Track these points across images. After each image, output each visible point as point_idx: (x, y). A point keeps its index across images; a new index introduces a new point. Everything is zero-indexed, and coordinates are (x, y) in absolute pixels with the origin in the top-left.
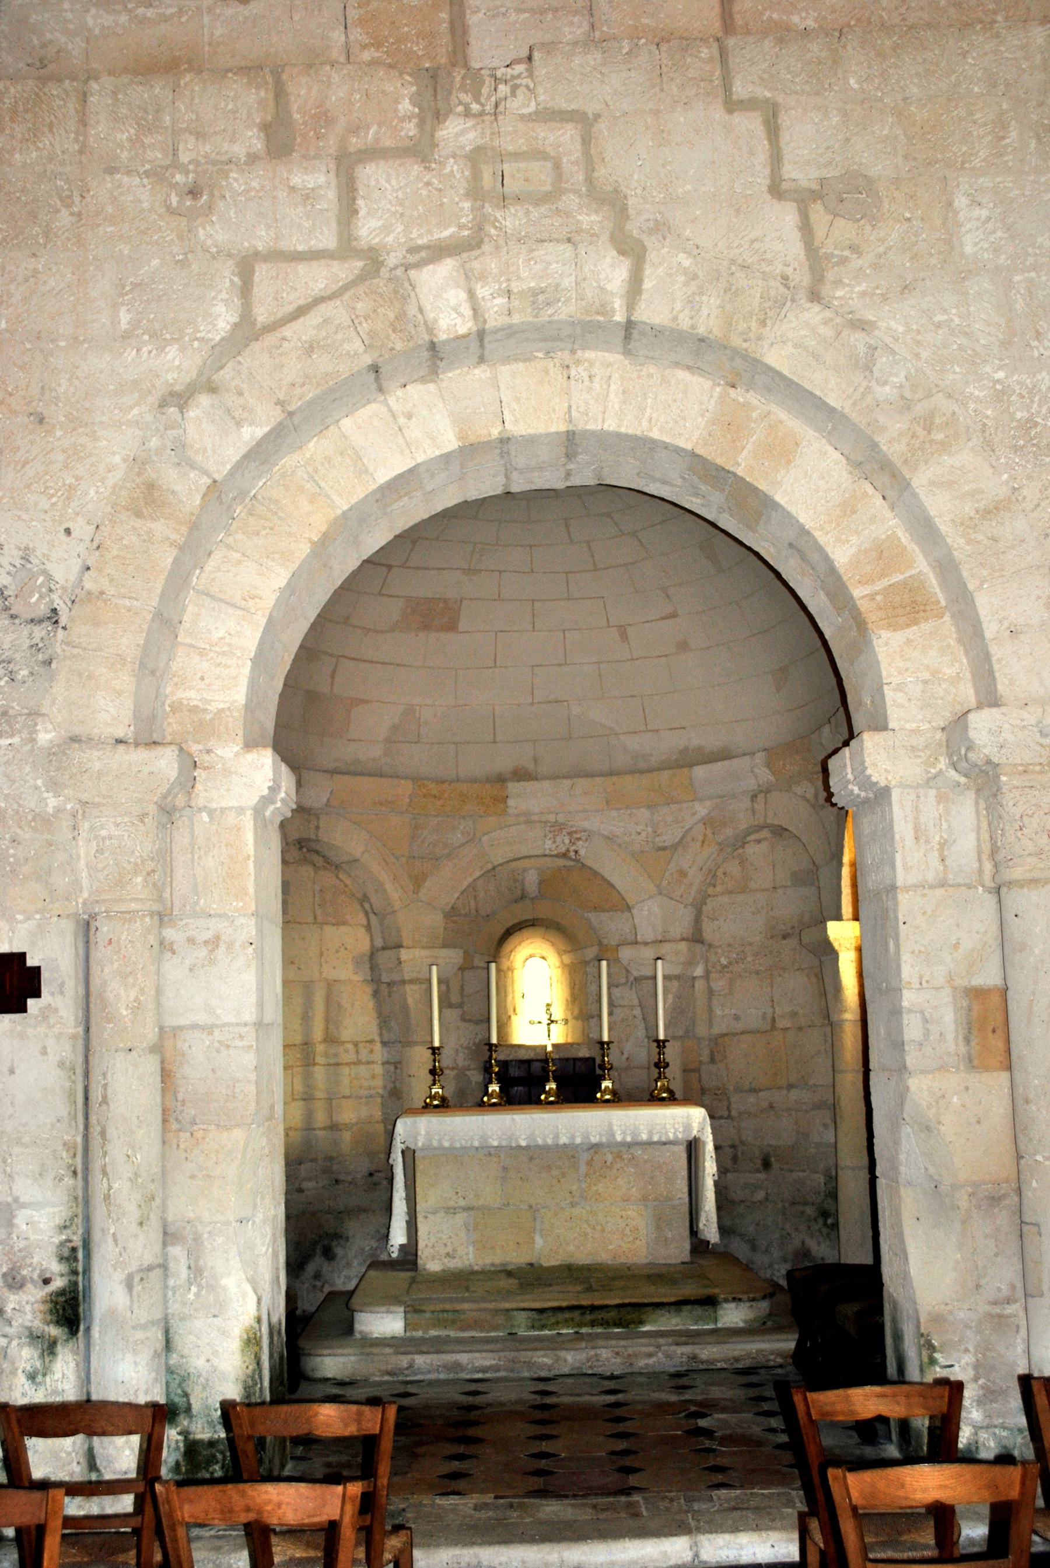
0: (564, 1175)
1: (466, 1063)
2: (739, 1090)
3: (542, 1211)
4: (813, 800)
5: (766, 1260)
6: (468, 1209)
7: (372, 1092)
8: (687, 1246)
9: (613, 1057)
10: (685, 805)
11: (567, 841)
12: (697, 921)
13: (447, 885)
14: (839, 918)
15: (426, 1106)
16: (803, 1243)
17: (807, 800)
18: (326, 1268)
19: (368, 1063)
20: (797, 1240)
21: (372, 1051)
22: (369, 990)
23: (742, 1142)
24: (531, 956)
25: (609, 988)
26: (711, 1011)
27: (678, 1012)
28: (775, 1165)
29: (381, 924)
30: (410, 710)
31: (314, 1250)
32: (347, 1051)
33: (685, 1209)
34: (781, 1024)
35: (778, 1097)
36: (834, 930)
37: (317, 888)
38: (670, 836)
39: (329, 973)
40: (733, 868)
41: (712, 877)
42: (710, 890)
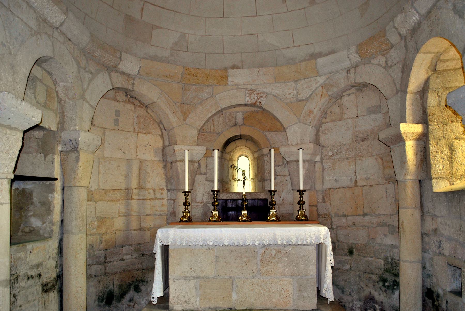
0: (249, 261)
1: (208, 200)
2: (337, 215)
3: (236, 280)
4: (384, 65)
5: (349, 298)
6: (198, 277)
7: (161, 213)
8: (315, 300)
9: (276, 198)
10: (312, 79)
11: (256, 98)
12: (317, 135)
13: (199, 117)
14: (405, 122)
15: (181, 221)
16: (370, 293)
17: (381, 66)
18: (136, 296)
19: (160, 199)
20: (367, 291)
21: (162, 194)
22: (162, 165)
23: (338, 241)
24: (241, 156)
25: (275, 167)
26: (323, 177)
27: (308, 177)
28: (355, 253)
29: (168, 134)
30: (183, 35)
31: (130, 288)
32: (149, 193)
33: (315, 280)
34: (360, 183)
35: (358, 219)
36: (403, 127)
37: (136, 116)
38: (304, 95)
39: (141, 156)
40: (336, 109)
41: (324, 114)
42: (324, 120)
